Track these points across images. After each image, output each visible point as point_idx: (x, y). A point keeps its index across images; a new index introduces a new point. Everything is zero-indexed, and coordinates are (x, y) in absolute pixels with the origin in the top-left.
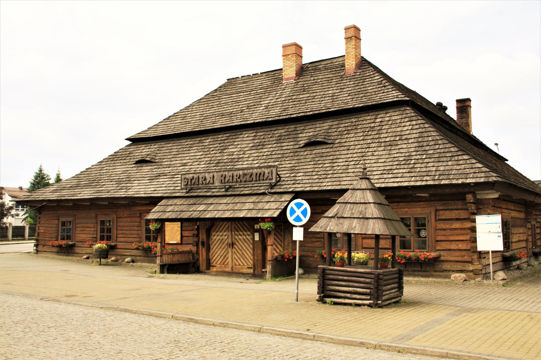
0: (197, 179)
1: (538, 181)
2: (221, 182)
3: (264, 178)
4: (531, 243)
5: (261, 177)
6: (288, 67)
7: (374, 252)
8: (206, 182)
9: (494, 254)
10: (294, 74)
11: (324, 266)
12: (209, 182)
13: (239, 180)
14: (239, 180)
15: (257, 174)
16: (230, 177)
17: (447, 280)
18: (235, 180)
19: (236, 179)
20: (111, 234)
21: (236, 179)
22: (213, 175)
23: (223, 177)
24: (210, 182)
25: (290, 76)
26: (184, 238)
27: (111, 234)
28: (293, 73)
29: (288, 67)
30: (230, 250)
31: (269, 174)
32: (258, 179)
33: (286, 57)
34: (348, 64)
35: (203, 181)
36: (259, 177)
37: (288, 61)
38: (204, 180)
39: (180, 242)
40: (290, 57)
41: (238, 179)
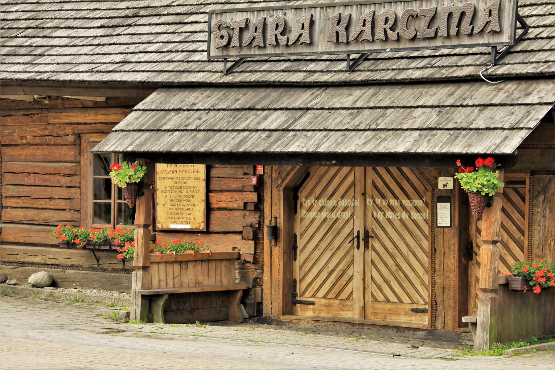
5: (466, 27)
14: (393, 35)
19: (385, 29)
21: (385, 29)
23: (344, 24)
24: (302, 40)
32: (453, 31)
35: (280, 37)
36: (459, 25)
41: (389, 31)
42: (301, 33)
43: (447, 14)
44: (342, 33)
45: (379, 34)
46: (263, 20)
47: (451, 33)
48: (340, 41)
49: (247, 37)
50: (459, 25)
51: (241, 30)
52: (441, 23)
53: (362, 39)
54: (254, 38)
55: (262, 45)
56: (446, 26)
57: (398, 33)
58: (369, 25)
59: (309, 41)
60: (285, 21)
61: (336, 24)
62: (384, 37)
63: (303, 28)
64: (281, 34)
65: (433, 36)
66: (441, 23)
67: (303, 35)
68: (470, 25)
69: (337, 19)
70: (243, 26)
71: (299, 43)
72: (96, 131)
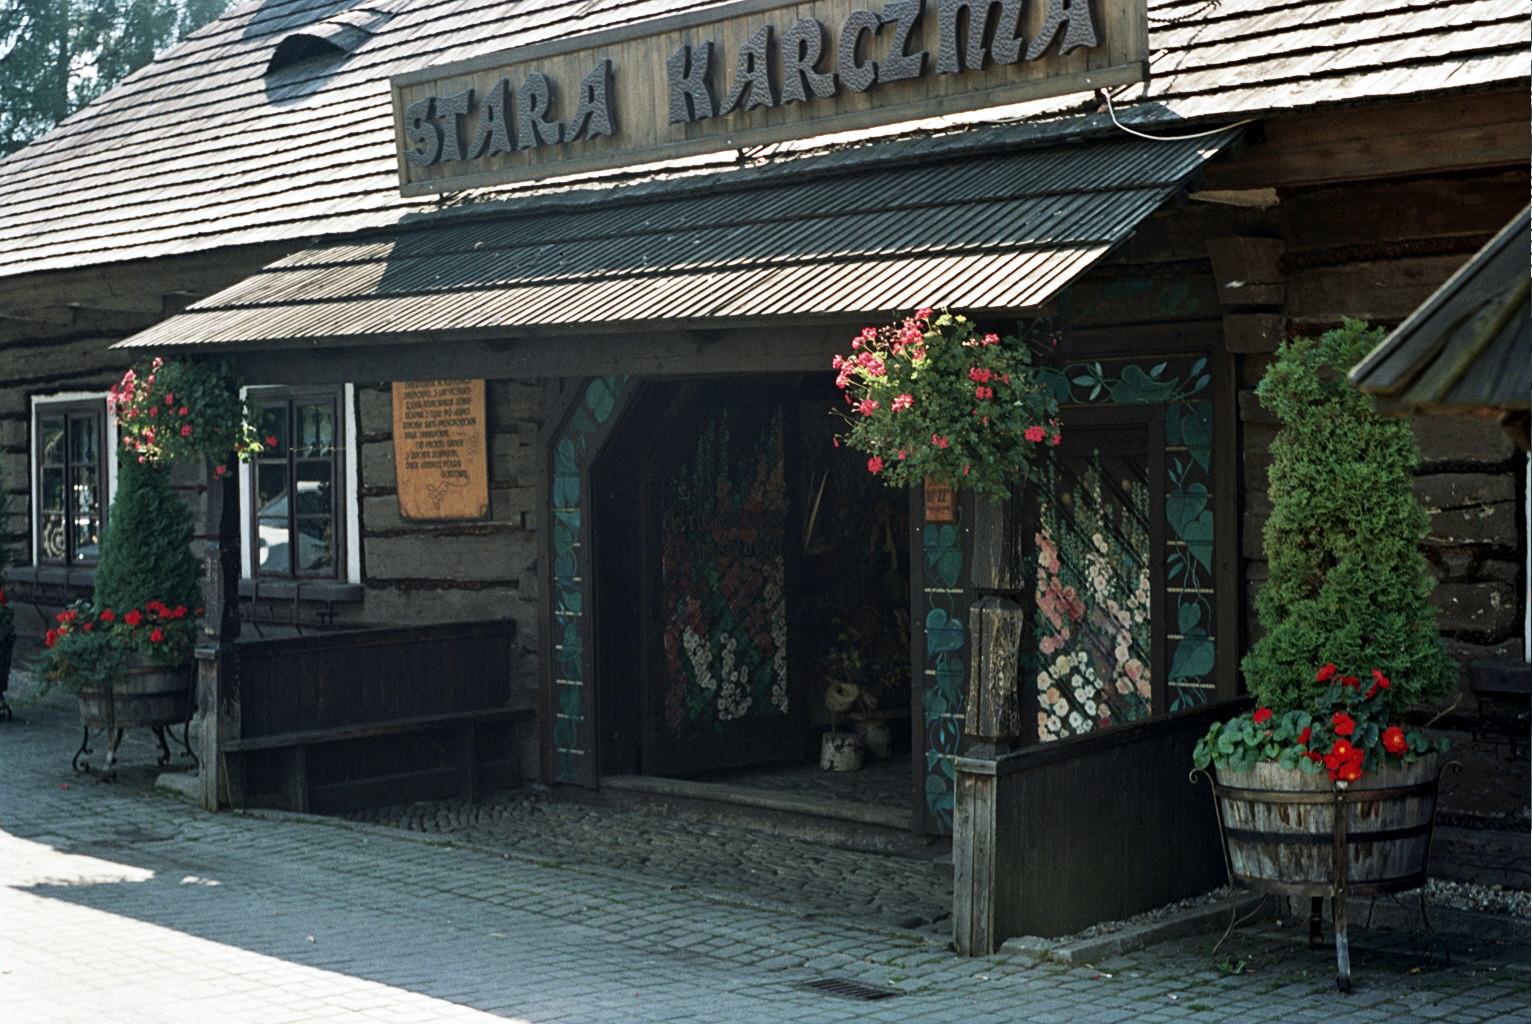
0: (498, 111)
2: (685, 114)
3: (1024, 49)
5: (1005, 46)
7: (1322, 831)
8: (562, 128)
11: (425, 719)
12: (1056, 42)
13: (822, 84)
14: (822, 84)
18: (792, 87)
19: (802, 73)
21: (802, 73)
22: (506, 83)
23: (699, 69)
24: (1071, 39)
31: (592, 99)
32: (975, 58)
35: (543, 126)
36: (987, 42)
38: (546, 117)
39: (288, 572)
41: (812, 75)
42: (1064, 18)
43: (954, 13)
44: (700, 94)
45: (792, 87)
46: (502, 87)
47: (968, 64)
48: (698, 114)
49: (476, 130)
50: (987, 42)
51: (460, 119)
52: (939, 44)
53: (750, 104)
54: (490, 134)
55: (1092, 42)
56: (954, 46)
57: (836, 77)
58: (761, 66)
59: (1094, 40)
60: (821, 25)
61: (681, 76)
62: (803, 94)
63: (751, 69)
64: (816, 68)
65: (916, 74)
66: (939, 44)
67: (1072, 22)
68: (1015, 38)
69: (682, 63)
70: (464, 111)
71: (1061, 52)
72: (577, 227)
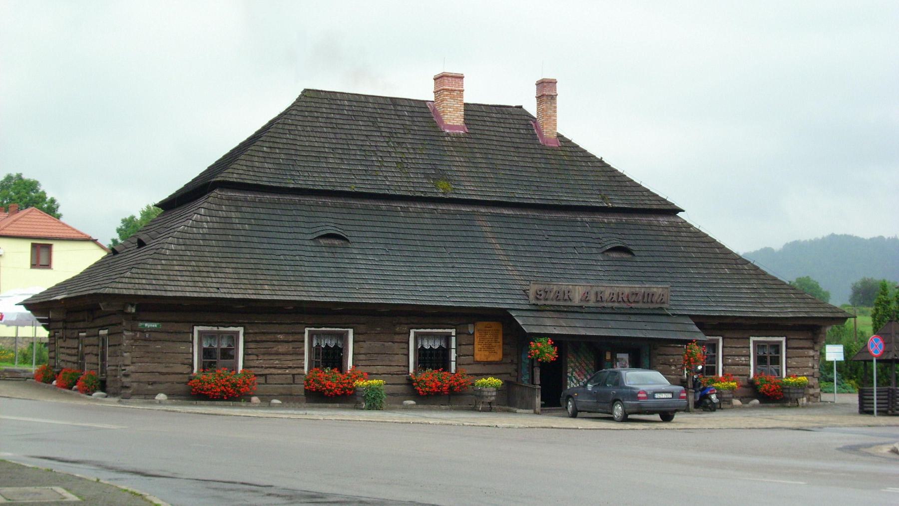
1: (74, 230)
4: (455, 350)
6: (453, 110)
9: (831, 390)
10: (461, 122)
15: (648, 294)
16: (613, 295)
17: (50, 385)
20: (202, 360)
25: (455, 124)
26: (191, 357)
27: (202, 360)
28: (459, 120)
29: (453, 110)
30: (495, 389)
32: (649, 300)
33: (449, 93)
34: (547, 130)
37: (452, 100)
40: (455, 94)
